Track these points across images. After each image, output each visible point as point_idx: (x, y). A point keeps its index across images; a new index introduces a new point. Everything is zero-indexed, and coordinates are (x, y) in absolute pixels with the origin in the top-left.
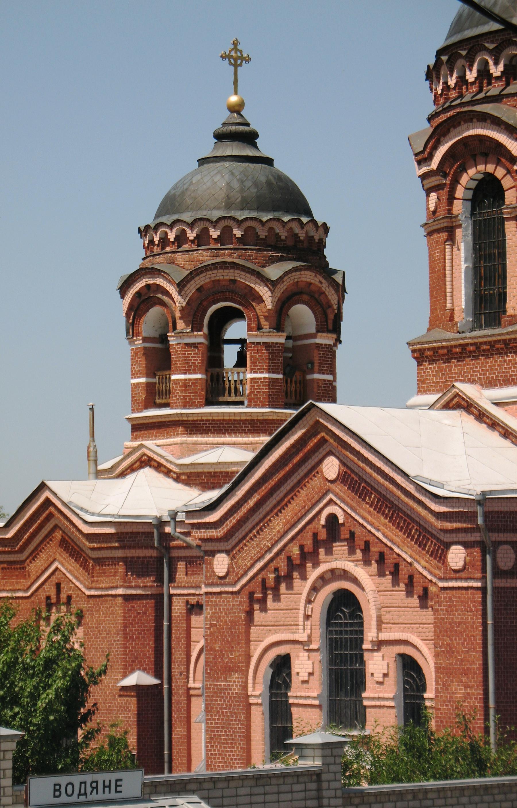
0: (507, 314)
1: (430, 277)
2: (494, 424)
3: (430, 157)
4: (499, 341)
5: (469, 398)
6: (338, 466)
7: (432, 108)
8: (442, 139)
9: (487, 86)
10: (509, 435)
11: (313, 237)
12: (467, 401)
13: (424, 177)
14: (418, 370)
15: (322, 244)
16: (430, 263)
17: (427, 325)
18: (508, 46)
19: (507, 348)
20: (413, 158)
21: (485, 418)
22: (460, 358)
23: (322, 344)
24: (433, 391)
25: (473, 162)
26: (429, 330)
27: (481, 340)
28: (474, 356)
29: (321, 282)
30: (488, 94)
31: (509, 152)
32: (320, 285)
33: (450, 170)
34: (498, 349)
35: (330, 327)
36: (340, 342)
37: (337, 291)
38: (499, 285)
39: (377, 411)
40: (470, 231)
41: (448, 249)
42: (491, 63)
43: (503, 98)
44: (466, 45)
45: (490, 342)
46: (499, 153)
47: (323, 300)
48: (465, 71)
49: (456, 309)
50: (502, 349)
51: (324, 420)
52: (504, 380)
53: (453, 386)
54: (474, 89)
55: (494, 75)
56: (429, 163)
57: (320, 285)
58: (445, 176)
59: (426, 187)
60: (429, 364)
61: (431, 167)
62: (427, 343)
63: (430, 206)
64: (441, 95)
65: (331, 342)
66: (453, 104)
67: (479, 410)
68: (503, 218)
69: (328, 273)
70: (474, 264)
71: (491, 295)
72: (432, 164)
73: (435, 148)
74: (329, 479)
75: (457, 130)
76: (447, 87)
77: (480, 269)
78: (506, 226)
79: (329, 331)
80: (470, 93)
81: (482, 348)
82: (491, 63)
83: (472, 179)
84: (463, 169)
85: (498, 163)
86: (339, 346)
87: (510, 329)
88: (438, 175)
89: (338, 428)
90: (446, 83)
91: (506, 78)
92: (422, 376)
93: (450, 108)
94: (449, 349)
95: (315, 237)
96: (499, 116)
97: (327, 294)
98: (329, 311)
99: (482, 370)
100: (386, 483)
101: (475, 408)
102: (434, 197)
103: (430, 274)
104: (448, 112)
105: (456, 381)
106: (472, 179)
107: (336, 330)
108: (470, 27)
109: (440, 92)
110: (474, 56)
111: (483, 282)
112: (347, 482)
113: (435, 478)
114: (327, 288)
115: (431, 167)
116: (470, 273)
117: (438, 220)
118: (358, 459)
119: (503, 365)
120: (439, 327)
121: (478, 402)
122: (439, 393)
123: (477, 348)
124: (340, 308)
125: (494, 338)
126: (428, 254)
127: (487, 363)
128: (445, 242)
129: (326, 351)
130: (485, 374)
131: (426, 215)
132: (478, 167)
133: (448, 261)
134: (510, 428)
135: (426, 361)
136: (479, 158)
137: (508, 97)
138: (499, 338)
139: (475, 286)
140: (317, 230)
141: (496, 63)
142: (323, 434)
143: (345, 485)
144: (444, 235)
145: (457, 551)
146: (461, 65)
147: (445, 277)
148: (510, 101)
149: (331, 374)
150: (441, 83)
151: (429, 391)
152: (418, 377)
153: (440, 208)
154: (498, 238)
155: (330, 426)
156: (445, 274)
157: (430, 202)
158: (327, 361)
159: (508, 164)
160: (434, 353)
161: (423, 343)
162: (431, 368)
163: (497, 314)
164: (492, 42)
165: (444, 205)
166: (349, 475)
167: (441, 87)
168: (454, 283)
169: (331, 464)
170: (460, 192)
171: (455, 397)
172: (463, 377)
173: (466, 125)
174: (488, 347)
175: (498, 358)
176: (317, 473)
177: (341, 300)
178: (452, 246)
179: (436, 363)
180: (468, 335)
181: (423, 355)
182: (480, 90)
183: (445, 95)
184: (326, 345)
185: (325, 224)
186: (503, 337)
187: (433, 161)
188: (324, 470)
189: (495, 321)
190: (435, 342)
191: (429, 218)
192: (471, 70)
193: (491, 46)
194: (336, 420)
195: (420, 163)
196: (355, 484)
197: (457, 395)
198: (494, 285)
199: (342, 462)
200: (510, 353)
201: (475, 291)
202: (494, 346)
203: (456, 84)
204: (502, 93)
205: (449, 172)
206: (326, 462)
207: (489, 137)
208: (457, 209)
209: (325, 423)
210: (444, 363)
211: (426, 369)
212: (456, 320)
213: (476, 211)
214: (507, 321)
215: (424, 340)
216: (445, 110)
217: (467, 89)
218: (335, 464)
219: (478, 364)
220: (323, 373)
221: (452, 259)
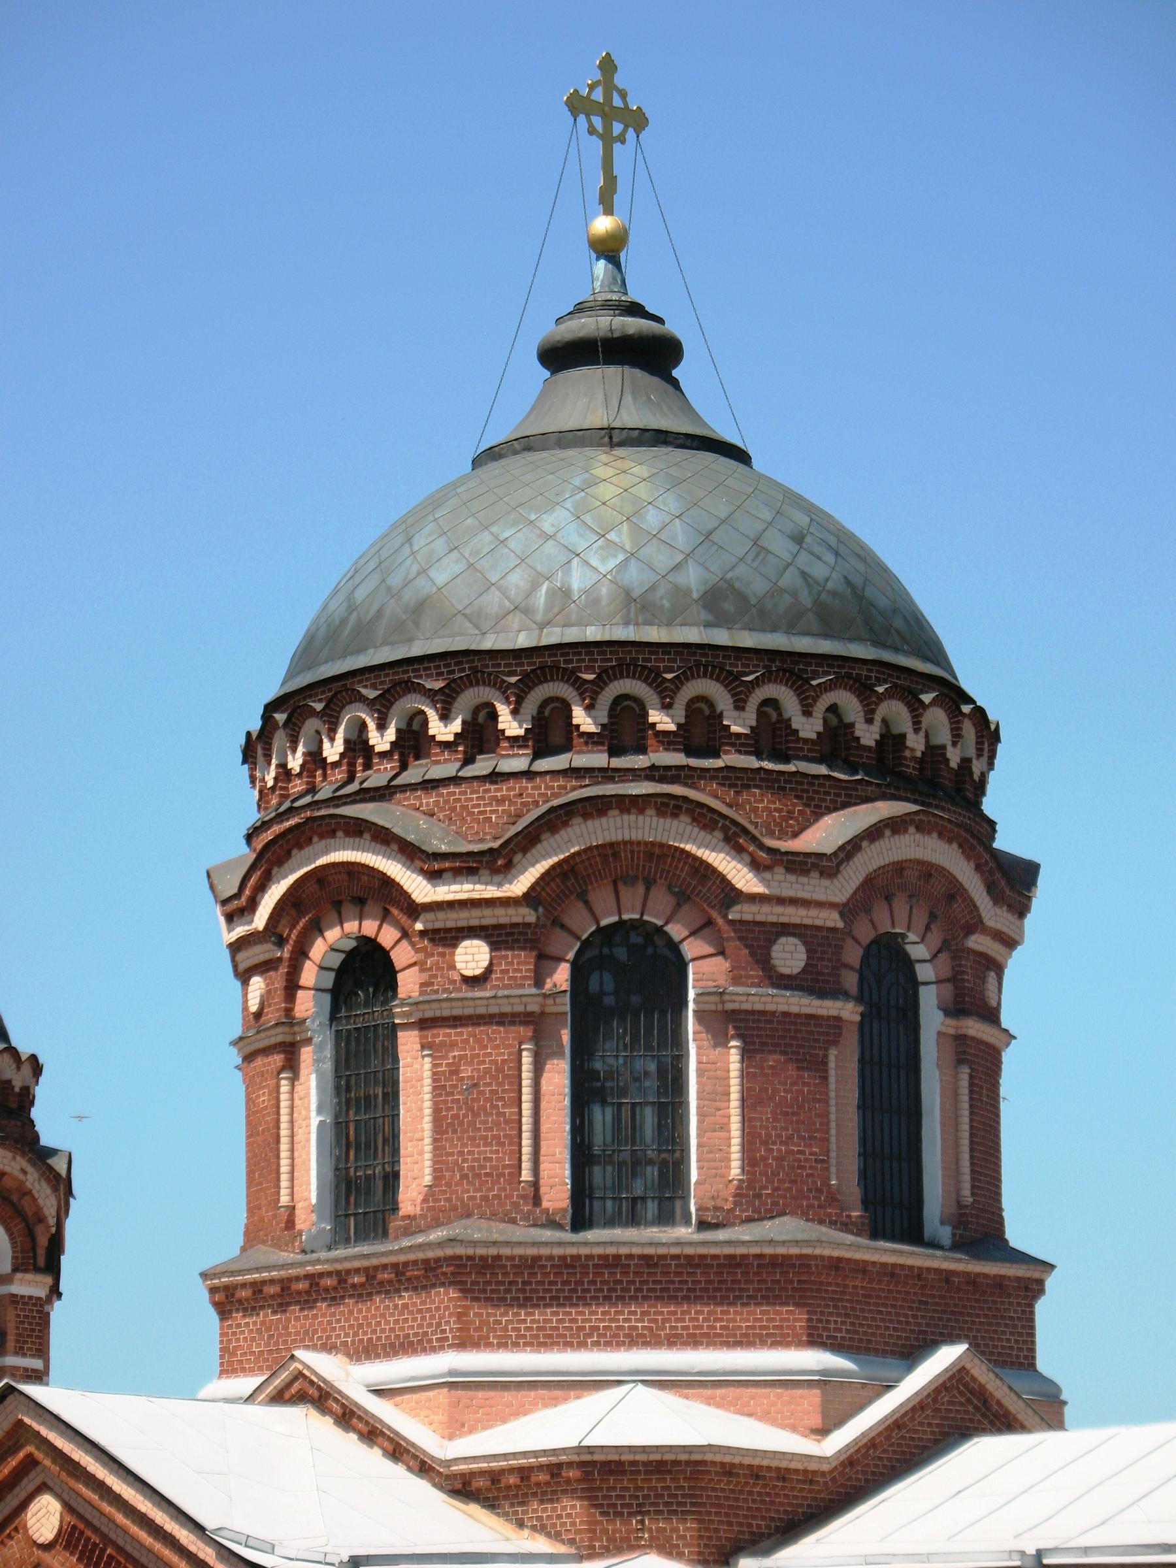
0: (401, 1213)
1: (248, 1144)
2: (373, 1433)
3: (252, 906)
4: (385, 1267)
5: (324, 1381)
6: (58, 1516)
7: (253, 816)
8: (275, 870)
9: (364, 771)
10: (401, 1455)
11: (9, 1082)
12: (319, 1388)
13: (236, 947)
14: (222, 1328)
15: (26, 1099)
16: (247, 1116)
17: (240, 1241)
18: (405, 694)
19: (399, 1281)
20: (218, 910)
21: (355, 1420)
22: (307, 1302)
23: (23, 1297)
24: (252, 1370)
25: (334, 916)
26: (243, 1249)
27: (348, 1265)
28: (334, 1299)
29: (24, 1172)
30: (365, 785)
31: (406, 895)
32: (22, 1177)
33: (291, 931)
34: (381, 1283)
35: (41, 1261)
36: (60, 1295)
37: (55, 1189)
38: (384, 1158)
39: (142, 1400)
40: (328, 1052)
41: (285, 1087)
42: (371, 725)
43: (395, 793)
44: (323, 692)
45: (366, 1269)
46: (383, 895)
47: (27, 1208)
48: (321, 742)
49: (299, 1205)
50: (390, 1282)
51: (32, 1419)
52: (392, 1345)
53: (293, 1356)
54: (339, 775)
55: (378, 749)
56: (249, 918)
57: (22, 1177)
58: (281, 942)
59: (241, 968)
60: (244, 1316)
61: (254, 926)
62: (240, 1272)
63: (250, 1003)
64: (273, 788)
65: (42, 1293)
66: (297, 804)
67: (343, 1406)
68: (395, 1026)
69: (41, 1156)
70: (336, 1117)
71: (368, 1178)
72: (256, 919)
73: (262, 888)
74: (40, 1541)
75: (307, 851)
76: (285, 773)
77: (347, 1127)
78: (400, 1041)
79: (37, 1270)
80: (331, 783)
81: (350, 1281)
82: (371, 725)
83: (333, 950)
84: (316, 928)
85: (385, 916)
86: (57, 1304)
87: (406, 1243)
88: (267, 942)
89: (62, 1434)
90: (283, 766)
91: (402, 755)
92: (229, 1341)
93: (291, 811)
94: (285, 1284)
95: (14, 1083)
96: (388, 825)
97: (36, 1195)
98: (39, 1230)
99: (351, 1326)
100: (158, 1546)
101: (336, 1400)
102: (257, 986)
103: (248, 1137)
104: (288, 819)
105: (298, 1347)
106: (333, 950)
107: (52, 1267)
108: (330, 659)
109: (270, 783)
110: (339, 713)
111: (352, 1153)
112: (76, 1547)
113: (258, 1531)
114: (36, 1184)
115: (254, 926)
116: (329, 1134)
117: (264, 1030)
118: (102, 1498)
119: (392, 1315)
120: (264, 1242)
121: (342, 1388)
122: (263, 1374)
123: (340, 1282)
124: (60, 1226)
125: (375, 1262)
126: (243, 1099)
127: (360, 1311)
128: (279, 1073)
129: (31, 1311)
130: (356, 1334)
131: (241, 1021)
132: (346, 925)
133: (284, 1111)
134: (405, 1439)
135: (237, 1310)
136: (348, 909)
137: (405, 791)
138: (385, 1260)
139: (338, 1160)
140: (18, 1068)
141: (382, 727)
142: (30, 1449)
143: (72, 1554)
144: (278, 1059)
145: (475, 950)
146: (312, 732)
147: (278, 1142)
148: (408, 799)
149: (40, 1357)
150: (273, 767)
151: (244, 1370)
152: (221, 1342)
153: (270, 1006)
154: (383, 1064)
155: (44, 1431)
156: (278, 1137)
157: (250, 996)
158: (33, 1330)
159: (404, 919)
160: (254, 1293)
161: (232, 1273)
162: (247, 1324)
163: (380, 1215)
164: (374, 687)
165: (278, 1001)
166: (82, 1533)
167: (273, 774)
168: (296, 1154)
169: (43, 1511)
170: (309, 975)
171: (295, 1379)
172: (312, 1339)
173: (323, 842)
174: (363, 1279)
175: (382, 1301)
176: (16, 1529)
177: (63, 1210)
178: (293, 1080)
179: (258, 1314)
180: (323, 1255)
181: (231, 1298)
182: (351, 779)
183: (282, 788)
184: (30, 1298)
185: (34, 1058)
186: (393, 1259)
187: (258, 913)
188: (29, 1524)
189: (375, 1230)
190: (257, 1270)
191: (246, 1026)
192: (332, 740)
193: (371, 694)
194: (57, 1418)
195: (230, 918)
196: (92, 1551)
197: (300, 1375)
198: (375, 1159)
199: (68, 1507)
200: (406, 1290)
201: (337, 1169)
202: (374, 1277)
203: (302, 766)
204: (393, 783)
205: (289, 935)
206: (33, 1507)
207: (367, 867)
208: (303, 1008)
209: (36, 1426)
210: (274, 1312)
211: (239, 1326)
212: (298, 1227)
213: (339, 1011)
214: (400, 1227)
215: (234, 1267)
216: (280, 817)
217: (325, 775)
218: (52, 1511)
219: (342, 1313)
220: (24, 1355)
221: (292, 1107)
